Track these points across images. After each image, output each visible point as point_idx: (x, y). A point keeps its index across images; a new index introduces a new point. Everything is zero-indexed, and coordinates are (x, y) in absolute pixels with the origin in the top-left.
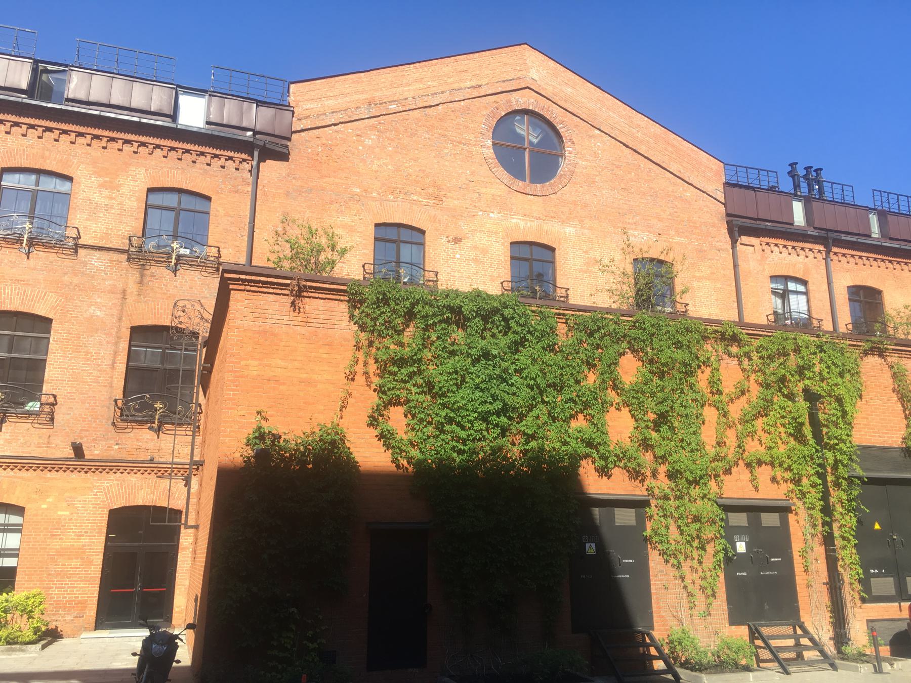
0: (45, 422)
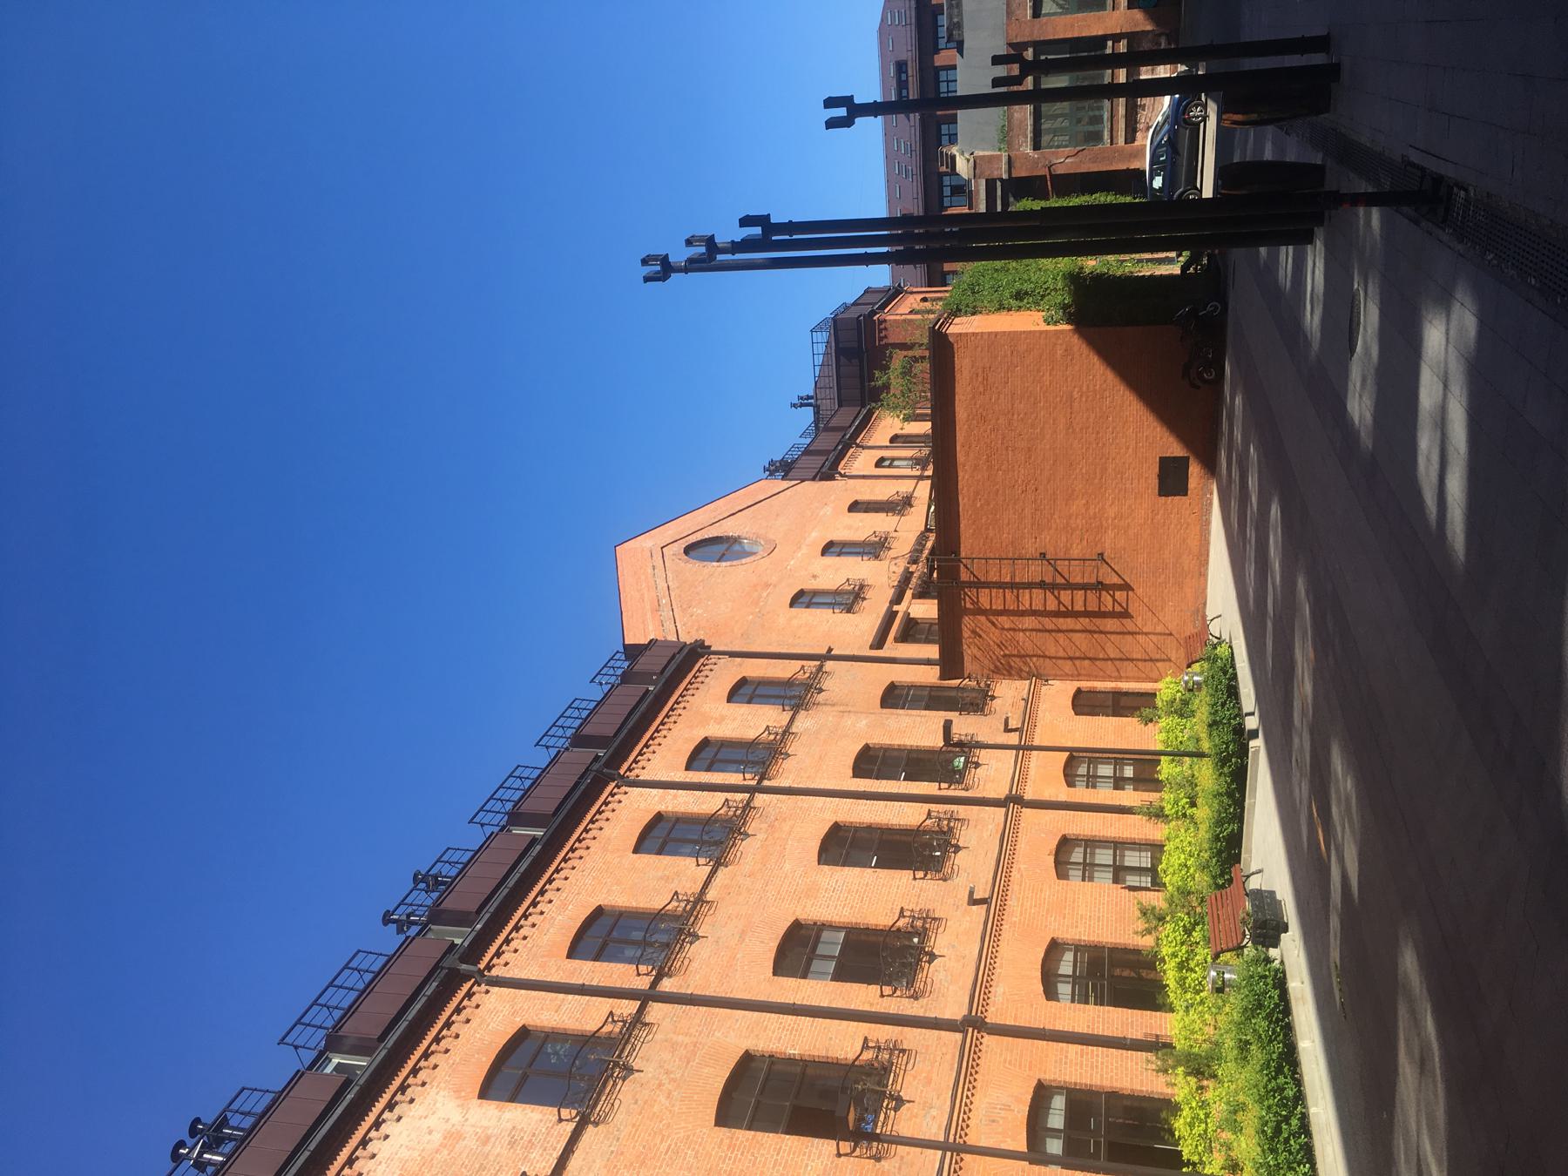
0: (905, 1057)
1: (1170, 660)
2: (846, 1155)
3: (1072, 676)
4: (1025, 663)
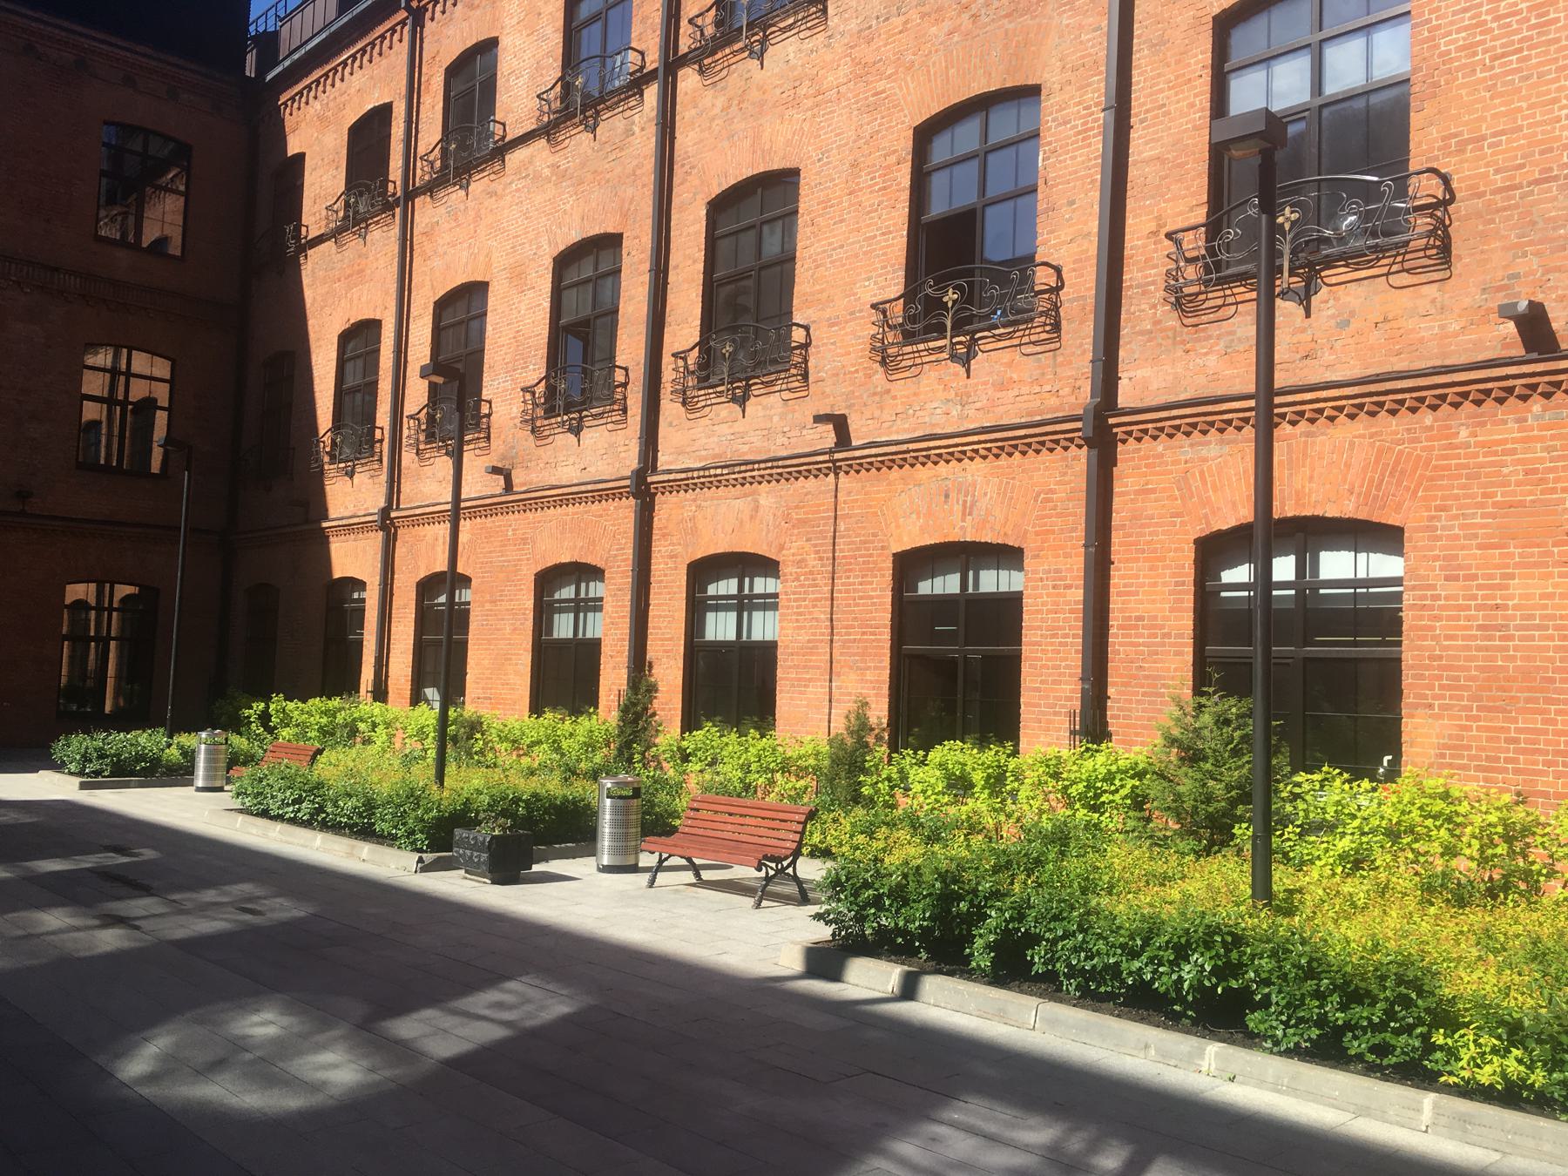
0: (1044, 336)
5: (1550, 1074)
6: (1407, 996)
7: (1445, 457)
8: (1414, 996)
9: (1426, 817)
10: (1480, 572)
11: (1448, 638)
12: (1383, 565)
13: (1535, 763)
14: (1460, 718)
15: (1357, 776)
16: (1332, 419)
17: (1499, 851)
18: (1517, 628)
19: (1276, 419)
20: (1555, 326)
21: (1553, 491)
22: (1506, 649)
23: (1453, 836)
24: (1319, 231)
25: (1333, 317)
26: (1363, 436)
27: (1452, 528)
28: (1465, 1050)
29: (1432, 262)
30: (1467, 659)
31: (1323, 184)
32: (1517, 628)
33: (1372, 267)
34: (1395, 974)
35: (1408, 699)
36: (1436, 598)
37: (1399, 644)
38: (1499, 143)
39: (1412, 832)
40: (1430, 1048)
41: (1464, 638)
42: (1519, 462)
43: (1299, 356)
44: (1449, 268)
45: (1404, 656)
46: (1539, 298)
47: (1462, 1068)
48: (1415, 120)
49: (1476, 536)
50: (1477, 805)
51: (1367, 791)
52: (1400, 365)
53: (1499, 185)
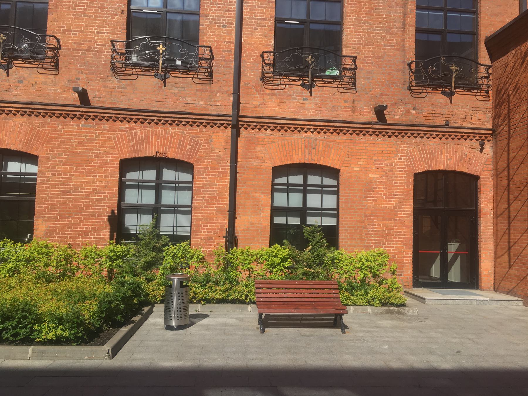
0: (349, 86)
1: (510, 267)
2: (263, 60)
3: (496, 169)
4: (504, 120)
5: (70, 332)
6: (25, 315)
7: (54, 134)
8: (28, 315)
9: (39, 254)
10: (63, 173)
11: (51, 194)
12: (31, 168)
13: (76, 234)
14: (54, 221)
15: (17, 241)
16: (15, 115)
17: (63, 263)
18: (74, 192)
19: (240, 126)
20: (90, 97)
21: (86, 149)
22: (70, 198)
23: (48, 260)
24: (13, 46)
25: (17, 78)
26: (26, 123)
27: (54, 158)
28: (44, 329)
29: (350, 87)
30: (57, 201)
31: (16, 30)
32: (74, 192)
33: (32, 64)
34: (22, 309)
35: (37, 215)
36: (48, 181)
37: (35, 196)
38: (76, 34)
39: (34, 259)
40: (32, 331)
41: (57, 194)
42: (77, 139)
43: (4, 90)
44: (58, 71)
45: (36, 200)
46: (85, 87)
47: (43, 335)
48: (49, 18)
49: (62, 161)
50: (56, 249)
51: (20, 247)
52: (40, 100)
53: (75, 48)
